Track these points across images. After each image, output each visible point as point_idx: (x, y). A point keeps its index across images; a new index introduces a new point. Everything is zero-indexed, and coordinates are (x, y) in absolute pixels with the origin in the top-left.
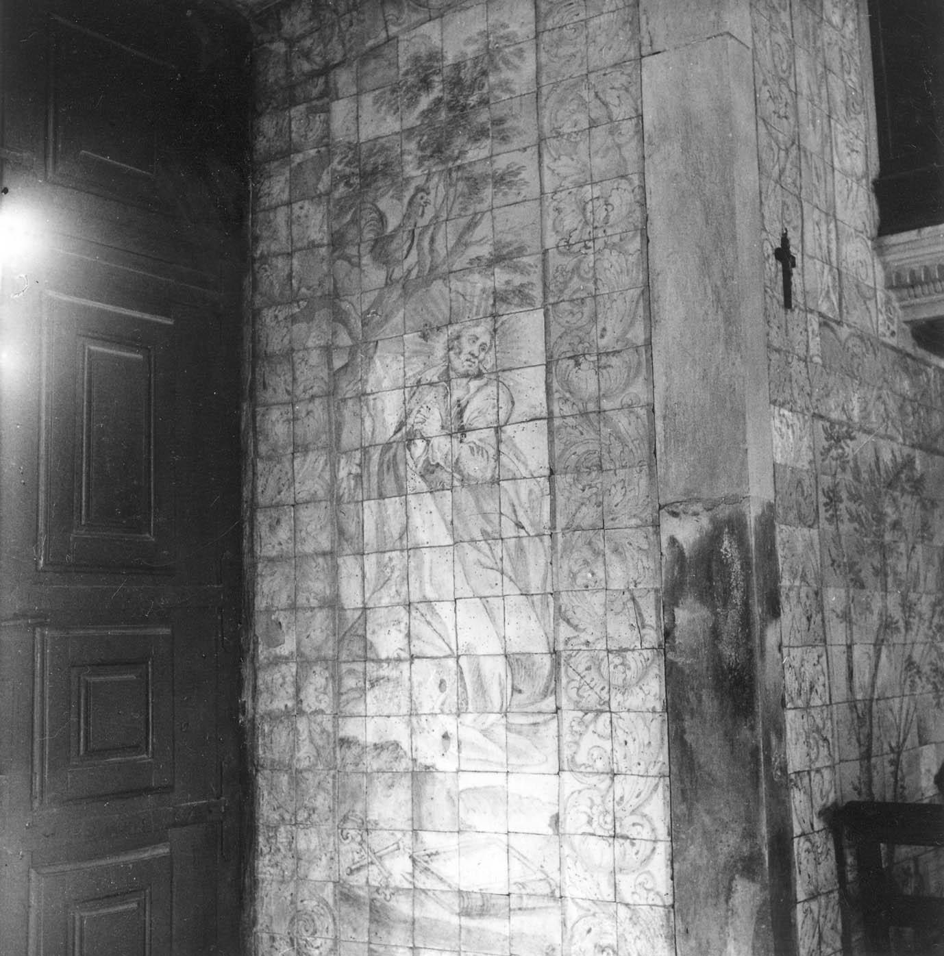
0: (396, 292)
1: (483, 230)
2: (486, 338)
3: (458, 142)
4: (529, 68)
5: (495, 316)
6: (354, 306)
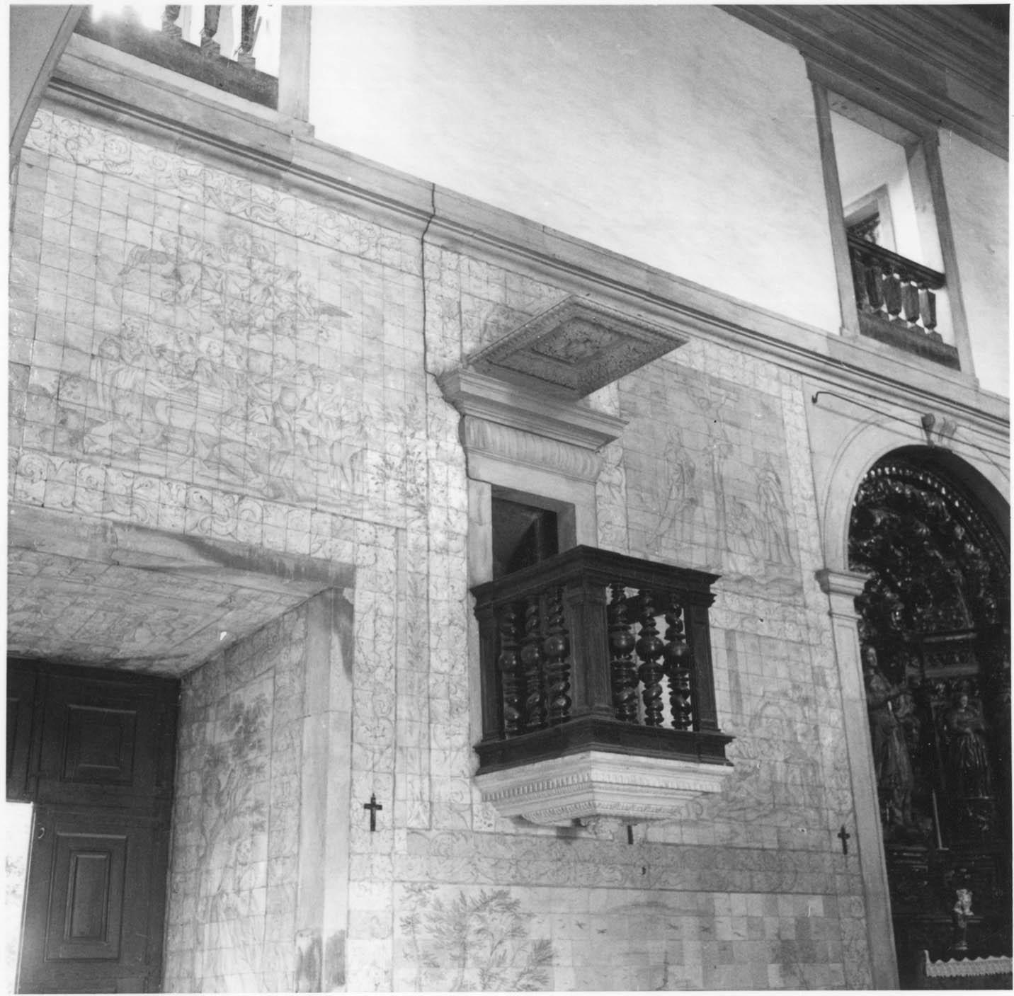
0: (222, 821)
1: (251, 795)
2: (249, 846)
3: (246, 749)
4: (270, 716)
5: (252, 835)
6: (209, 824)
